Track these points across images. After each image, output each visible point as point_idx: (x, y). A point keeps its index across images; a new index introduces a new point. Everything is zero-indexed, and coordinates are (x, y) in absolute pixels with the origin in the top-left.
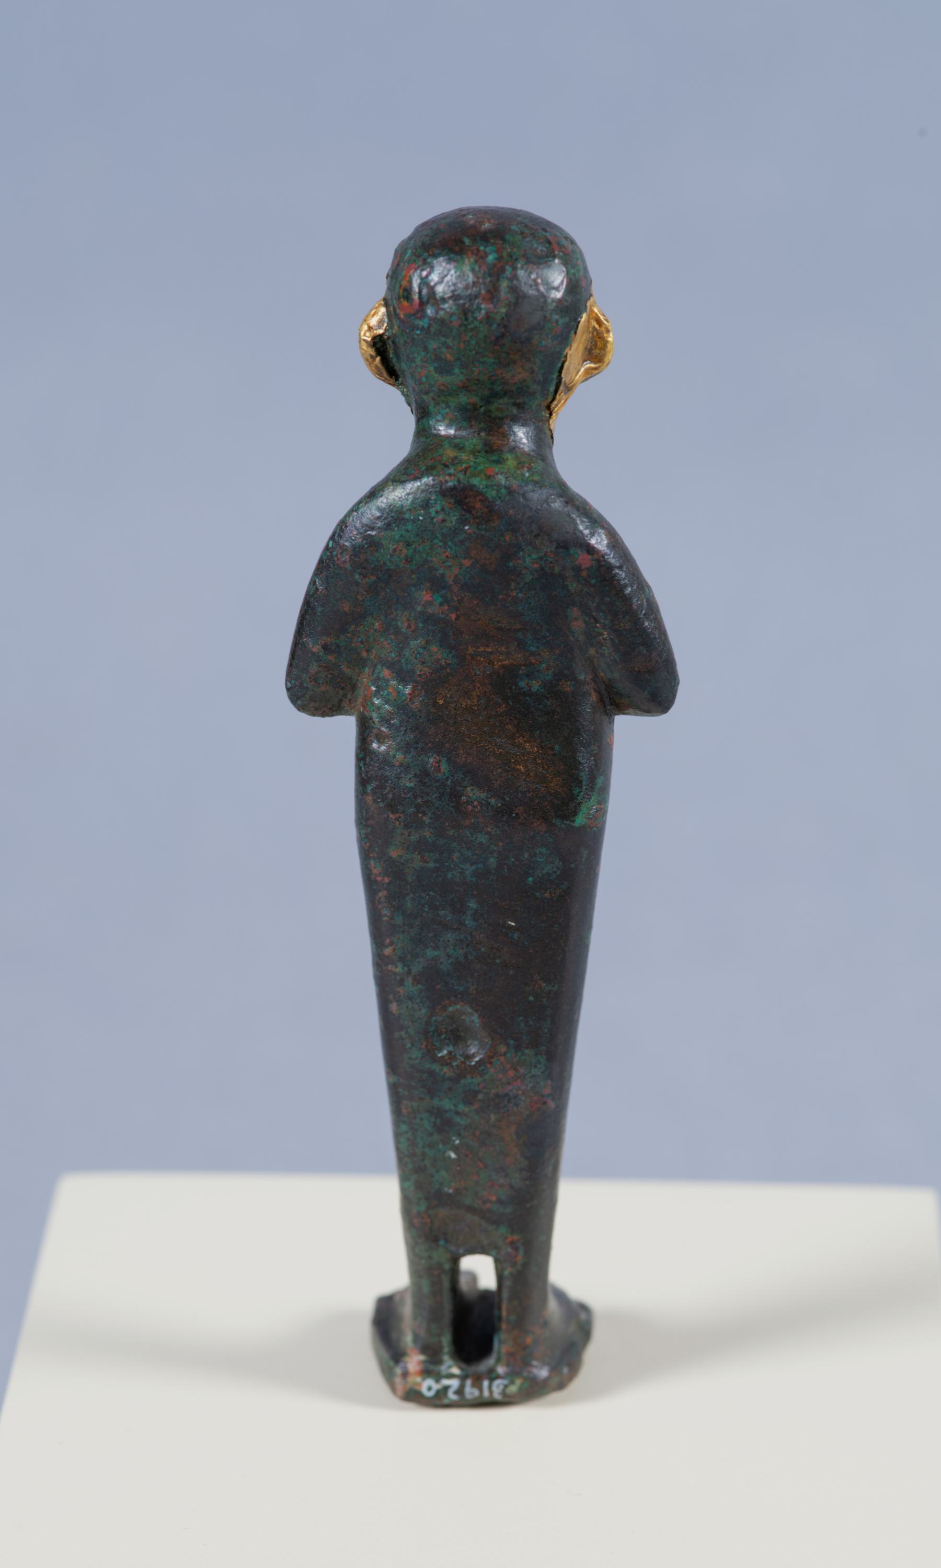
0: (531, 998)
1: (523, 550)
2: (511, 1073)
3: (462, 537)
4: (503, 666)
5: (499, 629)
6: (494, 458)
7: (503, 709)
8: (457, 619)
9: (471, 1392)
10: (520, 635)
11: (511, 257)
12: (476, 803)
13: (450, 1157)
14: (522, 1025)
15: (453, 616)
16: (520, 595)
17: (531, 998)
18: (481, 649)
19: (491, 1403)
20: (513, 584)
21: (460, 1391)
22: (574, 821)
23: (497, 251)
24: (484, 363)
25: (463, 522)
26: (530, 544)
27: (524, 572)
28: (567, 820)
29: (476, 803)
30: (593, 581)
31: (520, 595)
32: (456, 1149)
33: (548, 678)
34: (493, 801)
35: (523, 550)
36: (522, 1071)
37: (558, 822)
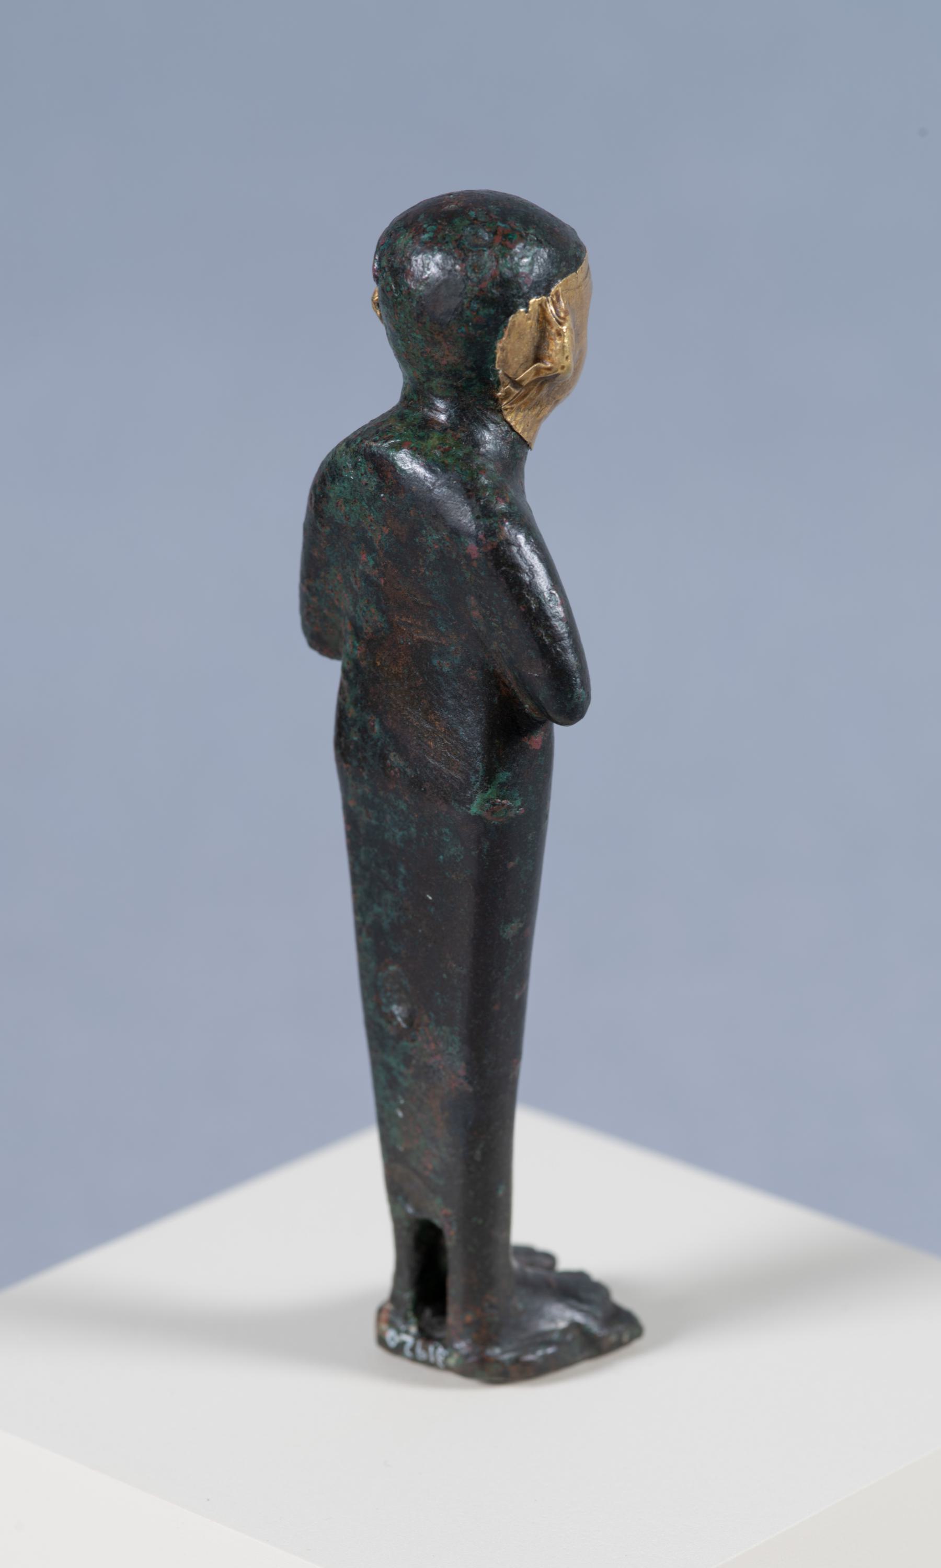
0: (445, 976)
1: (425, 529)
2: (433, 1046)
3: (379, 503)
4: (420, 641)
5: (415, 602)
6: (421, 434)
7: (420, 682)
8: (385, 584)
9: (420, 1352)
10: (431, 612)
11: (444, 239)
12: (397, 769)
13: (396, 1116)
14: (439, 1001)
15: (382, 581)
16: (427, 573)
17: (445, 976)
18: (404, 619)
19: (428, 1363)
20: (421, 561)
21: (413, 1349)
22: (469, 809)
23: (435, 232)
24: (414, 338)
25: (380, 488)
26: (430, 524)
27: (428, 550)
28: (464, 806)
29: (397, 769)
30: (483, 574)
31: (427, 573)
32: (402, 1108)
33: (456, 662)
34: (408, 771)
35: (425, 529)
36: (441, 1045)
37: (456, 805)
